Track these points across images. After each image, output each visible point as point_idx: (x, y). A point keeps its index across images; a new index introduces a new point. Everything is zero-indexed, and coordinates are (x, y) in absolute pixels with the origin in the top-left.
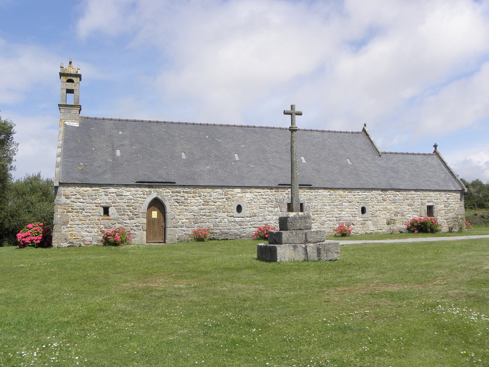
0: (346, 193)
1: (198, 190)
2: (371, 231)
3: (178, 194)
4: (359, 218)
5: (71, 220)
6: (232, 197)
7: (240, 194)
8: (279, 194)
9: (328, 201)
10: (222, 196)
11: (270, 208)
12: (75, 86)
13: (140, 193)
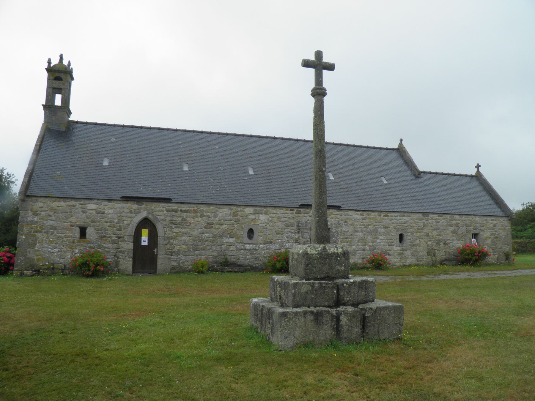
0: (382, 217)
1: (199, 209)
2: (409, 263)
3: (174, 213)
4: (396, 248)
5: (39, 242)
6: (243, 219)
7: (253, 216)
8: (301, 217)
9: (361, 226)
10: (230, 217)
11: (290, 234)
12: (64, 84)
13: (126, 211)
